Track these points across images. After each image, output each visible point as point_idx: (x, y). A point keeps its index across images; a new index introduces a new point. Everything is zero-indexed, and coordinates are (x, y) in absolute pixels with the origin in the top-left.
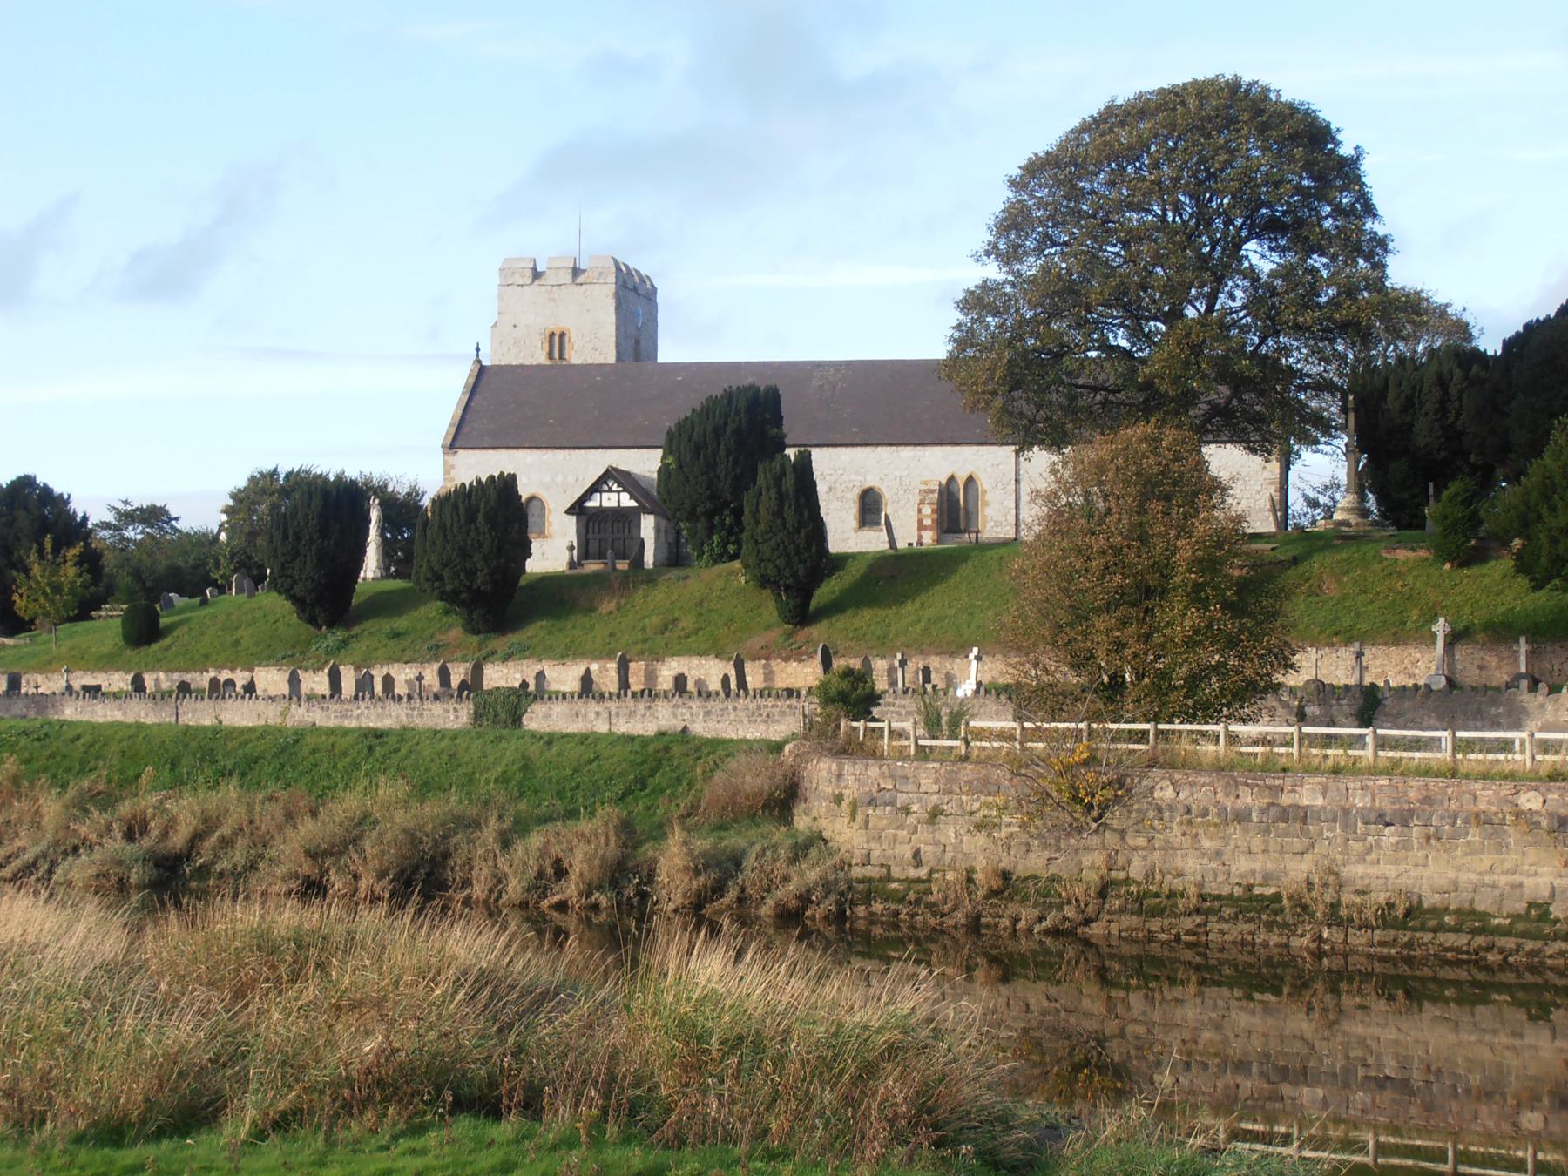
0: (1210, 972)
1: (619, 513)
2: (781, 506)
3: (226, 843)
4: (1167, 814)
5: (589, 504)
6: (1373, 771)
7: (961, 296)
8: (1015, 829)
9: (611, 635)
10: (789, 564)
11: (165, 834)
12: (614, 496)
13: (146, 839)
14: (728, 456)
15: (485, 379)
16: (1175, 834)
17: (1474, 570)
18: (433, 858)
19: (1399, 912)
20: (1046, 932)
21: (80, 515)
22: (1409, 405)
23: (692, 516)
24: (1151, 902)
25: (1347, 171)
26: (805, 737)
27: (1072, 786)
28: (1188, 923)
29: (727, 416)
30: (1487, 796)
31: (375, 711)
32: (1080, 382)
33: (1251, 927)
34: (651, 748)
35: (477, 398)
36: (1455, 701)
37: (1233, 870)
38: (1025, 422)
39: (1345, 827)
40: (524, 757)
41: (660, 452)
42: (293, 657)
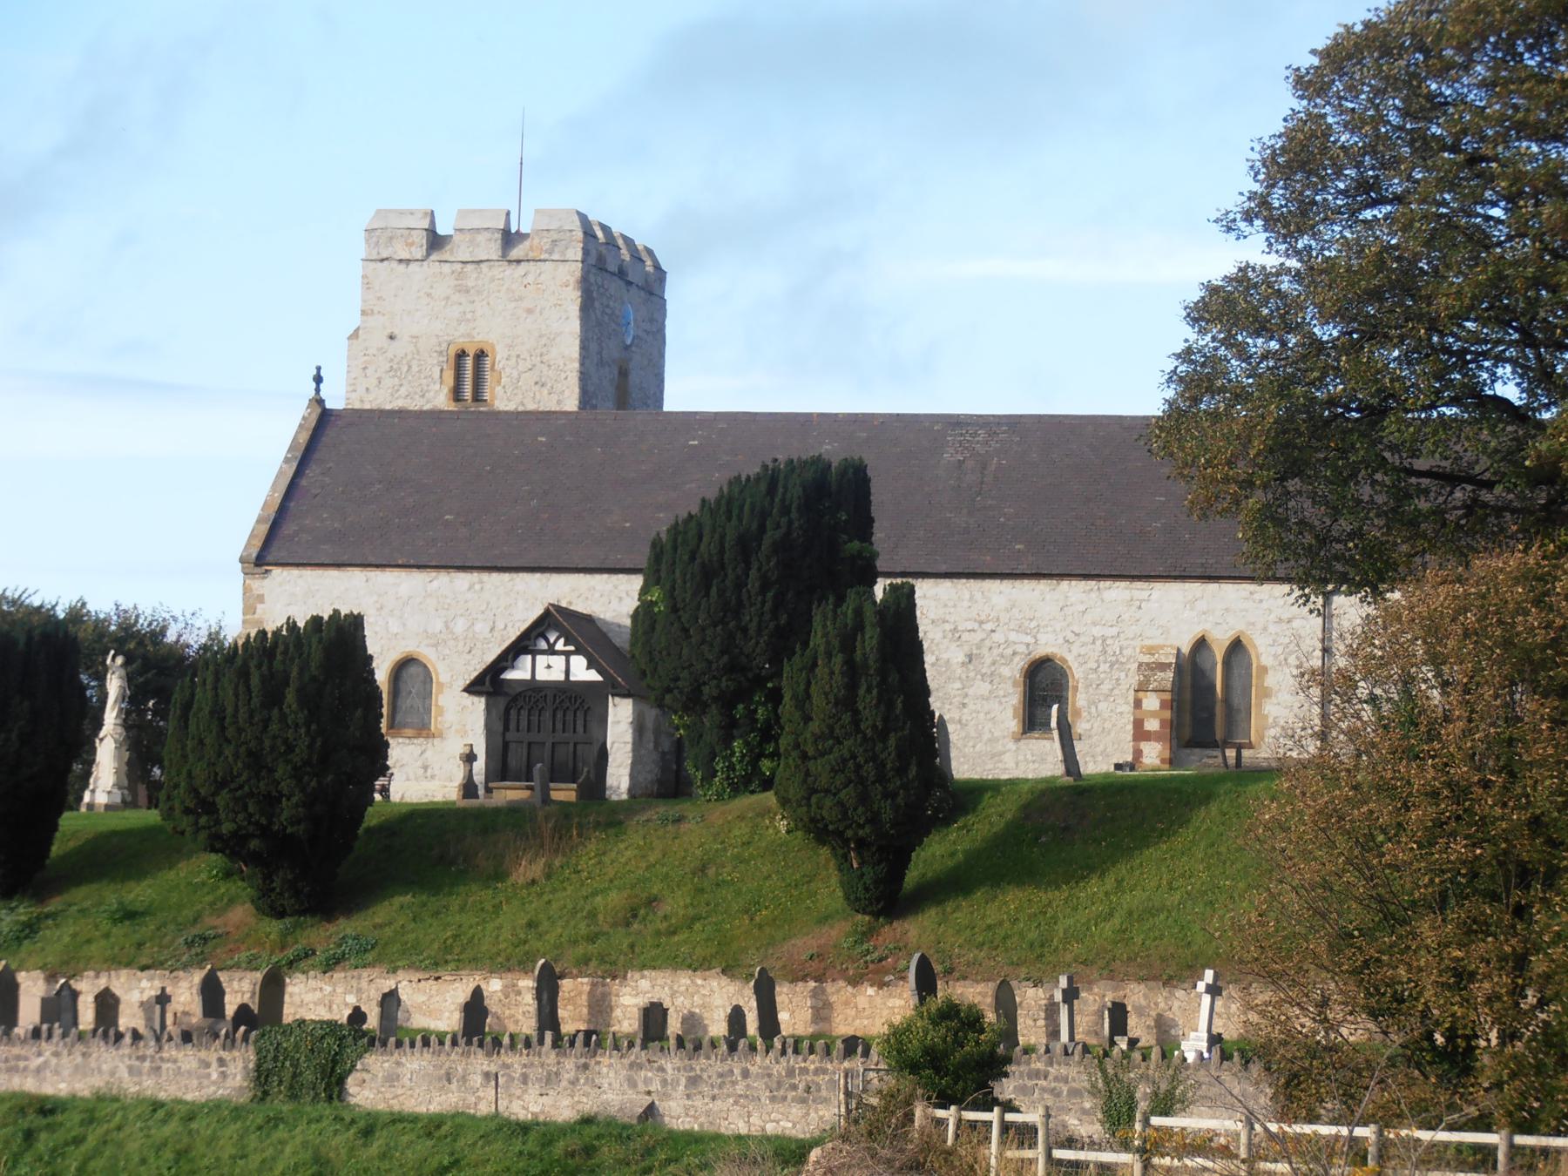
1: (567, 692)
2: (852, 686)
5: (510, 675)
7: (1196, 295)
9: (531, 925)
10: (864, 799)
12: (558, 662)
14: (764, 589)
15: (330, 434)
23: (693, 703)
26: (845, 1138)
31: (70, 1060)
32: (1421, 464)
34: (559, 1149)
35: (312, 472)
38: (1308, 539)
41: (637, 581)
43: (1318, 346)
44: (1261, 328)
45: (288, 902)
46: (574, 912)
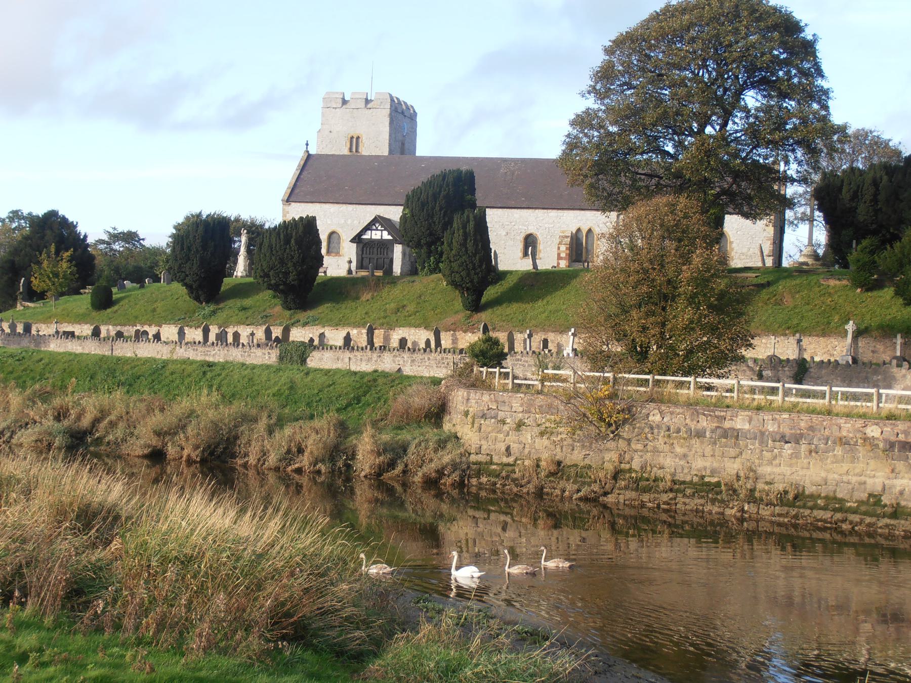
0: (678, 528)
2: (465, 240)
3: (113, 425)
4: (656, 431)
5: (364, 237)
6: (781, 410)
7: (573, 117)
8: (564, 436)
10: (468, 275)
11: (79, 418)
12: (379, 233)
13: (67, 420)
14: (440, 210)
16: (660, 443)
17: (875, 293)
18: (228, 439)
19: (791, 496)
20: (580, 499)
21: (83, 234)
22: (855, 196)
23: (418, 245)
24: (644, 484)
25: (808, 49)
27: (599, 411)
28: (665, 497)
29: (441, 187)
30: (847, 428)
33: (702, 501)
34: (365, 380)
36: (856, 371)
37: (693, 466)
38: (605, 194)
39: (761, 443)
40: (291, 382)
42: (183, 320)
43: (610, 134)
44: (592, 127)
45: (292, 306)
46: (380, 309)
